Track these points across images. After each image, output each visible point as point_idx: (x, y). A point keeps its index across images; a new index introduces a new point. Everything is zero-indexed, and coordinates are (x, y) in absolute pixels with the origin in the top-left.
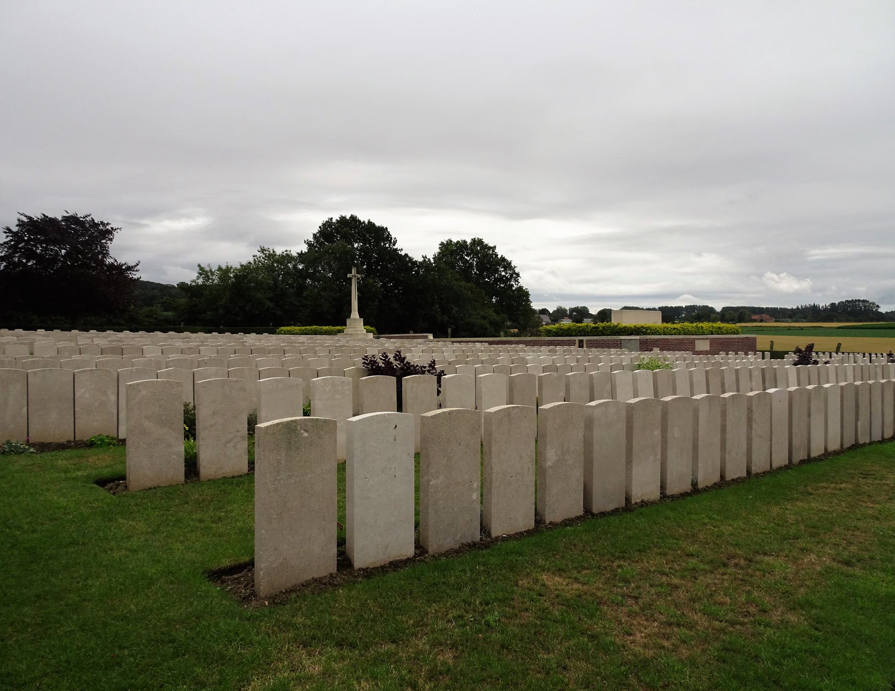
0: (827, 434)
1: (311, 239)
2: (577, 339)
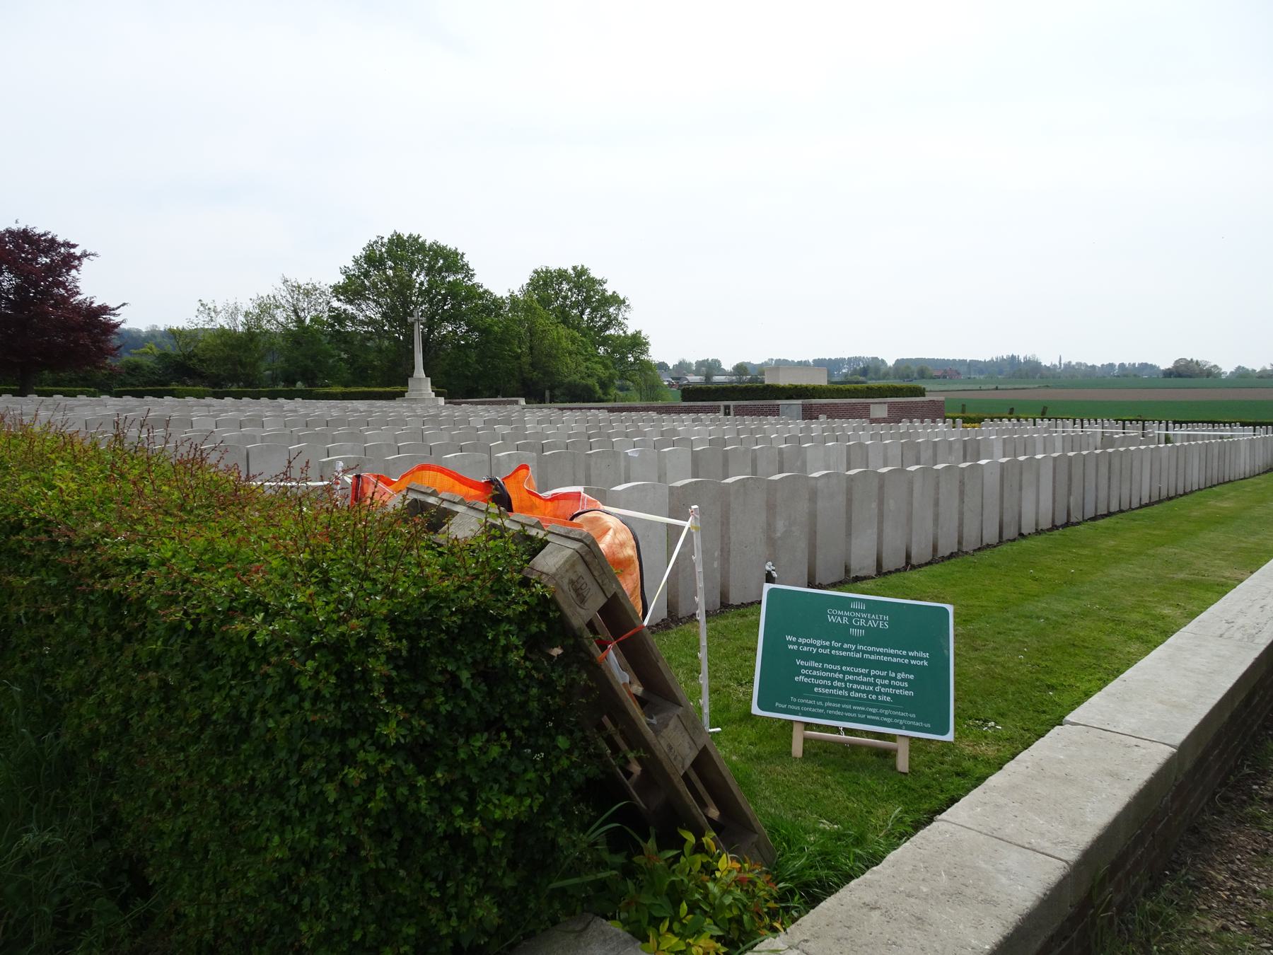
0: (1037, 506)
1: (351, 264)
2: (722, 404)
